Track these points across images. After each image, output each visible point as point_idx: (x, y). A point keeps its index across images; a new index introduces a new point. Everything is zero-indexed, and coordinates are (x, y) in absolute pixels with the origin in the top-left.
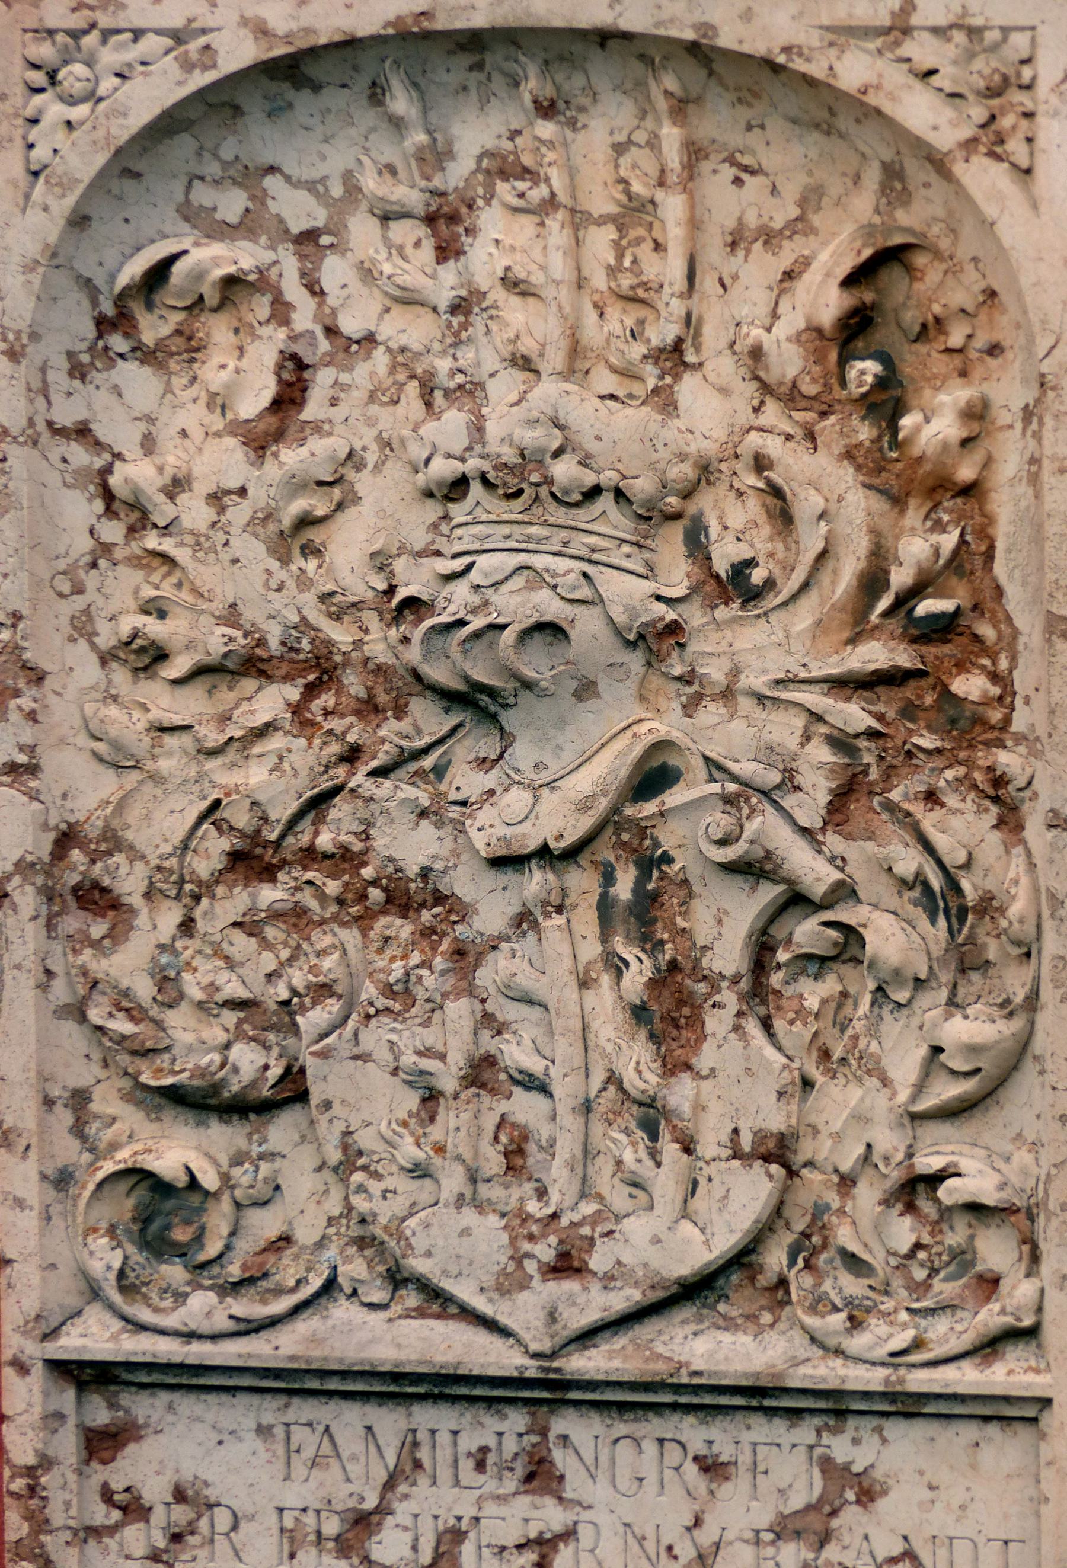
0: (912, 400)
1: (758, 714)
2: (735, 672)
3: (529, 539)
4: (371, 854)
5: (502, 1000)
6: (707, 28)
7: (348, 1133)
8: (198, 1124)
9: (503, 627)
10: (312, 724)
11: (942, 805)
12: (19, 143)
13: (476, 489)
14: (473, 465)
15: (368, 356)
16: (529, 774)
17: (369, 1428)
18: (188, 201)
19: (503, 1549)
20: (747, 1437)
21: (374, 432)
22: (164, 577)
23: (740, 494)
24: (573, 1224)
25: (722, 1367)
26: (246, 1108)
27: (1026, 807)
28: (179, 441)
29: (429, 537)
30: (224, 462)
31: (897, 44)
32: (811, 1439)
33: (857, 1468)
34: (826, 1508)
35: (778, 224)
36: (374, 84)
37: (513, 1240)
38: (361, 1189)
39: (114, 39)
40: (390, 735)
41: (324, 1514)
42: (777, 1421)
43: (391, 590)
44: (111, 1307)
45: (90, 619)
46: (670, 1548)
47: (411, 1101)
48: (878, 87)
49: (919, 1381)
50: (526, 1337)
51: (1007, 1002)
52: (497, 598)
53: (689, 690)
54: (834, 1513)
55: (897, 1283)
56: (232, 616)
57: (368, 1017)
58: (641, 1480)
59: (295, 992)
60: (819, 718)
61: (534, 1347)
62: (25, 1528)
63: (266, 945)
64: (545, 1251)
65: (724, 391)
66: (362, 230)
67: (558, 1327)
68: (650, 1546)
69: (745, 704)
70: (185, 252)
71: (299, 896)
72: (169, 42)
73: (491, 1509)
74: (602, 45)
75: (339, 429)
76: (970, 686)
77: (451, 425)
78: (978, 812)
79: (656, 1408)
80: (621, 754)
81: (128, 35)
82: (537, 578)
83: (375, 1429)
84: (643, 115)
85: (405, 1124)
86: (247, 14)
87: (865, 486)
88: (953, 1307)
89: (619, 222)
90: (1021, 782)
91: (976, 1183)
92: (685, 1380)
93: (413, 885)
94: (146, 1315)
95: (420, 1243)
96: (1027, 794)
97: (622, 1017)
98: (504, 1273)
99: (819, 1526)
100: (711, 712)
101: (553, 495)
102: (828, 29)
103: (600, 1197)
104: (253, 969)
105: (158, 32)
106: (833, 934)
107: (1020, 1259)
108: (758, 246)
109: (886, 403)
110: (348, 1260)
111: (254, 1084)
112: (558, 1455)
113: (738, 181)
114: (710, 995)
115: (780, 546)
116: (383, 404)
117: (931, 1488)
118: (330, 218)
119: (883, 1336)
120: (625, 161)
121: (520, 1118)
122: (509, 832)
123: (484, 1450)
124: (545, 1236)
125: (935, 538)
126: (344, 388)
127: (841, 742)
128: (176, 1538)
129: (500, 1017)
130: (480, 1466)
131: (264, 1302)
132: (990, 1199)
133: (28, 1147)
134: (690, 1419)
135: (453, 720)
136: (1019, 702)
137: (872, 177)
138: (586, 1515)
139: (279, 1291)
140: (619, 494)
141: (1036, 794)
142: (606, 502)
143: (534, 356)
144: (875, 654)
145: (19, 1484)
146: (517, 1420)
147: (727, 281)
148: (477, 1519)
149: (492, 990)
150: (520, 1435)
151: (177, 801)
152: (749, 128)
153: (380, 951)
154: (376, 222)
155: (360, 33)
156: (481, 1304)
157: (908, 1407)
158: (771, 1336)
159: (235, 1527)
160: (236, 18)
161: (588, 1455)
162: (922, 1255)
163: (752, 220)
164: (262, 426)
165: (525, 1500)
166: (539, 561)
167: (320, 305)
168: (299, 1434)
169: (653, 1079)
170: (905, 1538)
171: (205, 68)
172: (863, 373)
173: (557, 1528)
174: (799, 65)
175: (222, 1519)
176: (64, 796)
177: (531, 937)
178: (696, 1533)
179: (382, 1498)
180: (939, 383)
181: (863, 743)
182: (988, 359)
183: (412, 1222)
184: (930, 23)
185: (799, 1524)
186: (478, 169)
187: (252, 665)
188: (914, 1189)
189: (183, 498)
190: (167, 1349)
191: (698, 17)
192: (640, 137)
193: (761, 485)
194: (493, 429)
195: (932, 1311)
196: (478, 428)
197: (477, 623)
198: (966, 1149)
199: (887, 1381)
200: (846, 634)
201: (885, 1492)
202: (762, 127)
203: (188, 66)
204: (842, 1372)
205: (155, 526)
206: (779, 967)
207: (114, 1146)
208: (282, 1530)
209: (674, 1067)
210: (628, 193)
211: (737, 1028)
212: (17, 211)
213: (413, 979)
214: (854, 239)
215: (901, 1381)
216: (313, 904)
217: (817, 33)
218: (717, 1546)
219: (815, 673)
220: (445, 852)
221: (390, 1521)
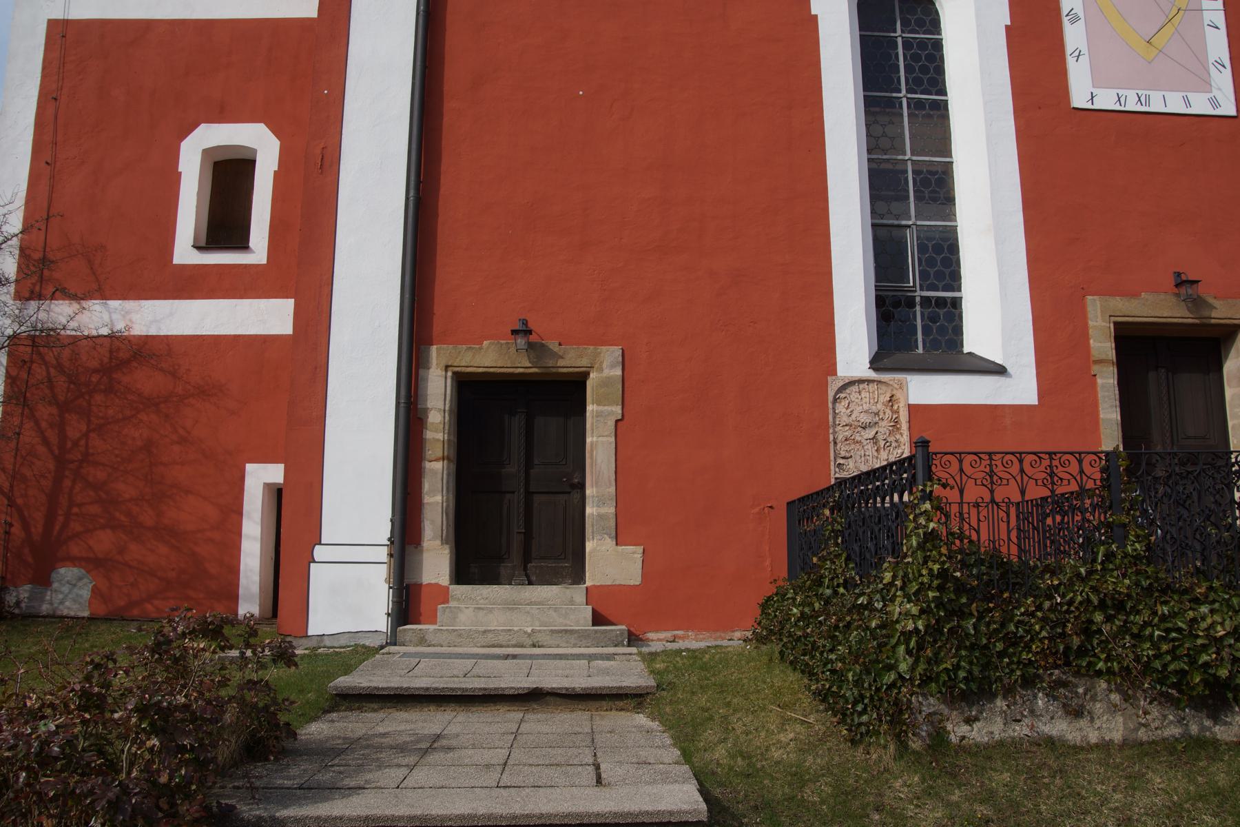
104: (847, 448)
214: (326, 753)
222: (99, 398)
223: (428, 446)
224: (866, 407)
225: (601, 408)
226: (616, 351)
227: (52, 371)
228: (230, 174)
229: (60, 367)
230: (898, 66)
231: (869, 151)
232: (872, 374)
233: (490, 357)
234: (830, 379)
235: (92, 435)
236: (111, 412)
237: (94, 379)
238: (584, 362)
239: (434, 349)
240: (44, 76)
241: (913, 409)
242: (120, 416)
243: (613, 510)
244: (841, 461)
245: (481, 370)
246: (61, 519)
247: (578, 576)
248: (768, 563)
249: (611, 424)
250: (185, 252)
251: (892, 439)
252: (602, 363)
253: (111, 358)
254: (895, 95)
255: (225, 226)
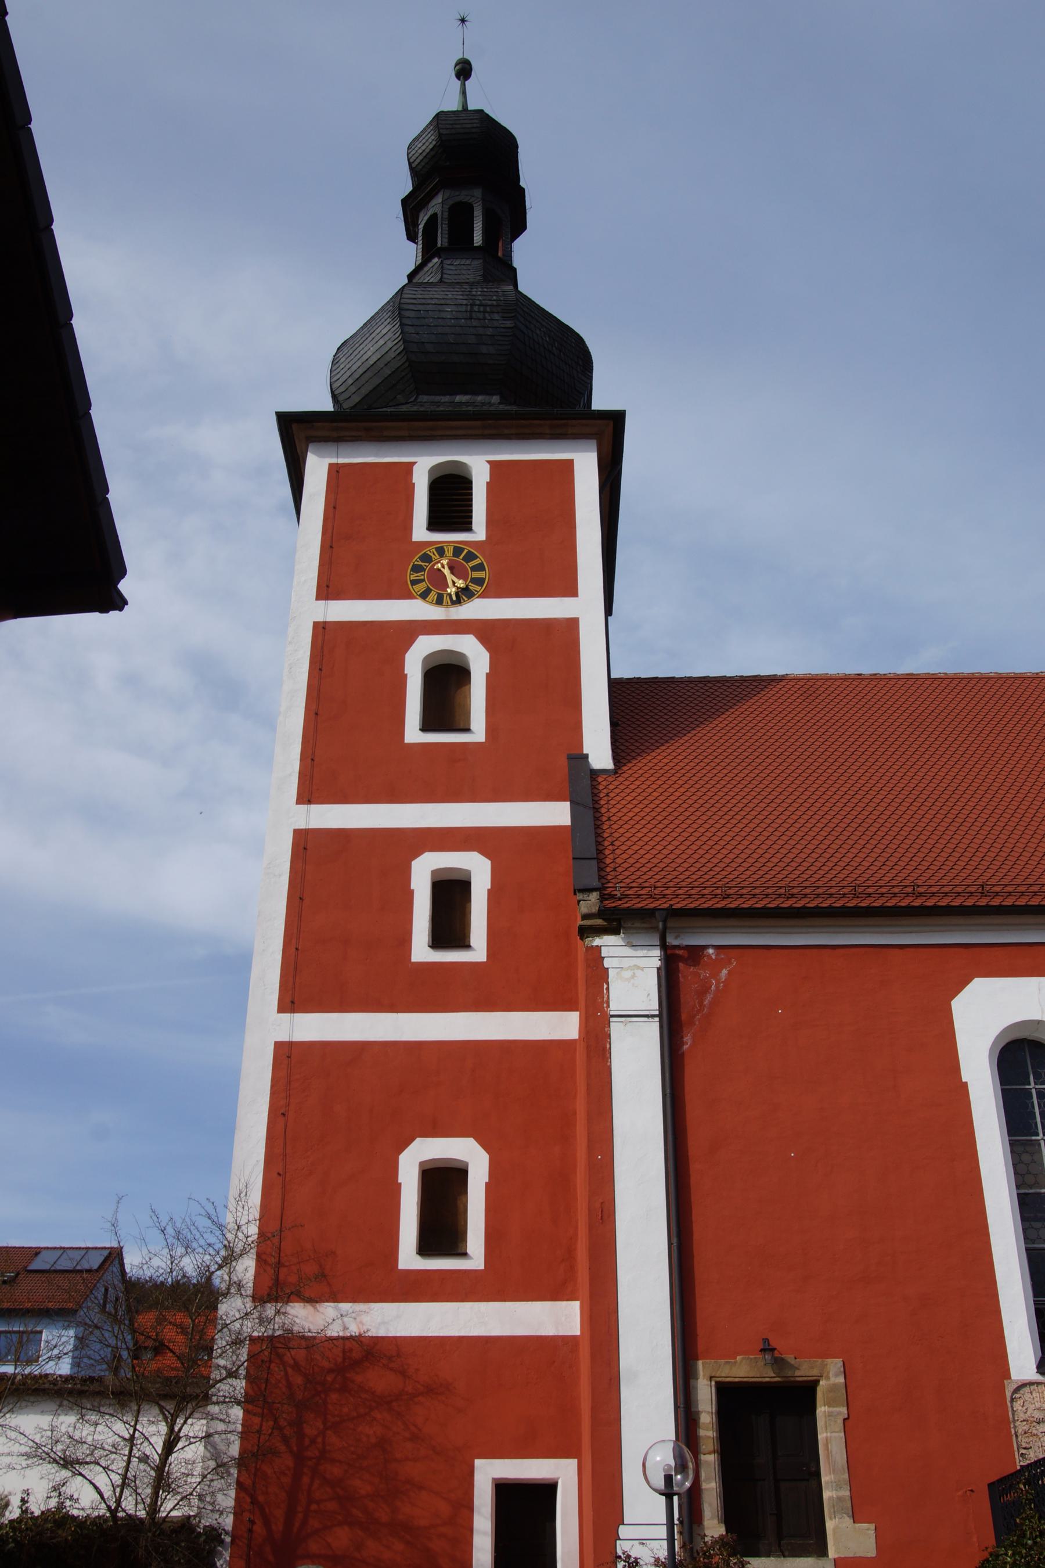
104: (1027, 1440)
222: (334, 1396)
223: (702, 1442)
224: (1038, 1405)
225: (831, 1409)
226: (839, 1362)
227: (290, 1370)
228: (443, 1184)
229: (296, 1366)
230: (1034, 1113)
231: (1018, 1187)
232: (1039, 1378)
233: (743, 1369)
235: (329, 1432)
236: (345, 1410)
237: (329, 1378)
238: (815, 1372)
239: (700, 1363)
240: (272, 1094)
242: (355, 1414)
243: (848, 1493)
244: (1024, 1451)
245: (737, 1380)
246: (300, 1516)
247: (820, 1549)
248: (975, 1539)
249: (840, 1421)
250: (408, 1257)
252: (828, 1373)
253: (344, 1359)
254: (1034, 1138)
255: (441, 1231)
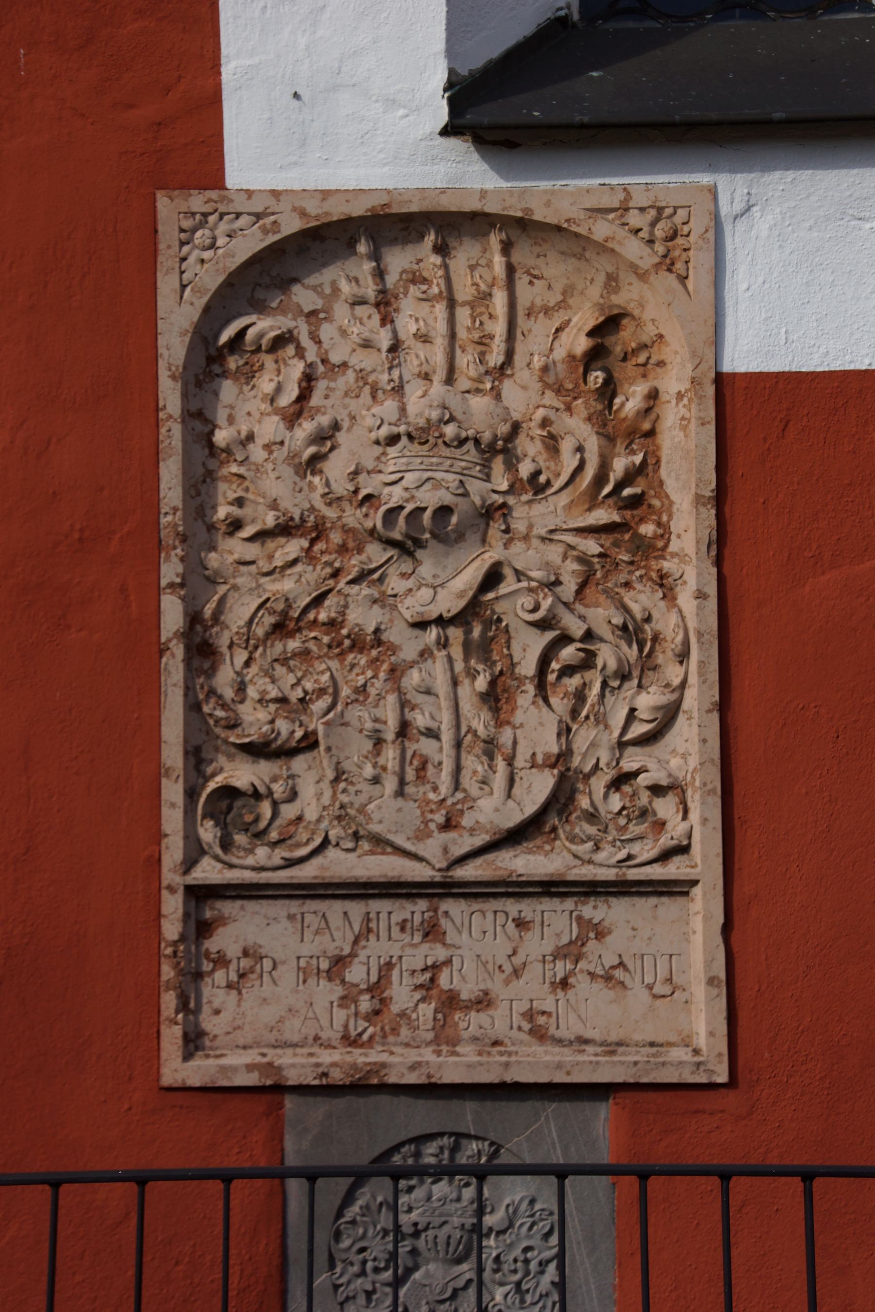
0: (619, 390)
1: (542, 547)
2: (531, 527)
3: (432, 464)
4: (346, 623)
5: (414, 693)
6: (527, 210)
7: (338, 763)
8: (253, 762)
9: (424, 509)
10: (315, 558)
11: (634, 589)
12: (177, 270)
13: (404, 440)
14: (402, 429)
15: (344, 374)
16: (430, 580)
17: (345, 913)
18: (252, 297)
19: (414, 971)
20: (540, 908)
21: (347, 412)
22: (239, 485)
23: (532, 438)
24: (454, 804)
25: (534, 872)
26: (287, 753)
27: (678, 589)
28: (246, 417)
29: (376, 463)
30: (270, 428)
31: (622, 216)
32: (572, 907)
33: (595, 921)
34: (581, 941)
35: (551, 304)
36: (351, 238)
37: (423, 813)
38: (344, 791)
39: (226, 218)
40: (354, 564)
41: (321, 959)
42: (555, 899)
43: (356, 492)
44: (217, 858)
45: (203, 509)
46: (500, 967)
47: (369, 745)
48: (613, 238)
49: (633, 874)
50: (434, 861)
51: (667, 685)
52: (419, 494)
53: (507, 536)
54: (583, 945)
55: (611, 827)
56: (274, 505)
57: (347, 704)
58: (485, 932)
59: (306, 693)
60: (571, 547)
61: (437, 866)
62: (172, 974)
63: (290, 670)
64: (439, 818)
65: (524, 388)
66: (341, 311)
67: (449, 855)
68: (490, 967)
69: (535, 542)
70: (254, 324)
71: (307, 644)
72: (254, 219)
73: (409, 951)
74: (472, 219)
75: (329, 411)
76: (647, 529)
77: (389, 407)
78: (653, 592)
79: (495, 895)
80: (477, 569)
81: (233, 216)
82: (438, 485)
83: (349, 914)
84: (485, 251)
85: (366, 757)
86: (296, 205)
87: (598, 433)
88: (642, 838)
89: (472, 305)
90: (677, 576)
91: (655, 775)
92: (515, 879)
93: (369, 638)
94: (235, 861)
95: (376, 816)
96: (679, 582)
97: (475, 699)
98: (418, 830)
99: (576, 952)
100: (518, 547)
101: (445, 443)
102: (587, 209)
103: (465, 791)
105: (249, 214)
106: (582, 654)
107: (678, 812)
108: (541, 315)
109: (608, 391)
110: (334, 827)
111: (288, 740)
112: (443, 921)
113: (531, 283)
114: (518, 687)
115: (552, 464)
116: (352, 398)
117: (634, 929)
118: (324, 305)
119: (609, 854)
120: (477, 274)
121: (425, 752)
122: (423, 609)
123: (405, 921)
124: (438, 810)
125: (630, 458)
126: (332, 390)
127: (583, 559)
128: (242, 976)
129: (413, 701)
130: (403, 929)
131: (291, 851)
132: (664, 782)
133: (178, 777)
134: (512, 900)
135: (389, 555)
136: (673, 537)
137: (601, 278)
138: (458, 952)
139: (298, 845)
140: (477, 442)
141: (685, 583)
142: (470, 445)
143: (431, 373)
144: (602, 516)
145: (169, 951)
146: (422, 905)
147: (526, 333)
148: (400, 957)
149: (410, 688)
150: (423, 913)
151: (246, 599)
152: (538, 256)
153: (351, 670)
154: (348, 306)
155: (354, 215)
156: (408, 846)
157: (622, 888)
158: (552, 856)
159: (274, 967)
160: (290, 207)
161: (458, 921)
162: (625, 813)
163: (538, 302)
164: (292, 410)
165: (426, 946)
166: (439, 475)
167: (320, 348)
168: (308, 918)
169: (493, 730)
170: (620, 956)
171: (275, 233)
172: (597, 377)
173: (442, 959)
174: (574, 228)
175: (267, 964)
176: (193, 598)
177: (430, 661)
178: (513, 958)
179: (352, 949)
180: (632, 381)
181: (596, 560)
182: (624, 364)
183: (371, 806)
184: (639, 205)
185: (565, 951)
186: (401, 279)
187: (285, 529)
188: (621, 780)
189: (251, 447)
190: (249, 876)
191: (523, 205)
192: (483, 262)
193: (545, 434)
194: (412, 410)
195: (631, 840)
196: (403, 410)
197: (409, 507)
198: (647, 758)
199: (617, 875)
200: (586, 506)
201: (610, 933)
202: (545, 256)
203: (265, 231)
204: (594, 871)
205: (236, 460)
206: (553, 671)
207: (214, 775)
208: (299, 968)
209: (500, 723)
210: (478, 290)
211: (534, 703)
212: (177, 305)
213: (369, 684)
215: (624, 874)
216: (315, 649)
217: (582, 212)
218: (525, 964)
219: (571, 526)
220: (386, 620)
221: (356, 960)
224: (421, 404)
232: (466, 175)
234: (168, 208)
241: (734, 398)
244: (242, 774)
251: (602, 616)
